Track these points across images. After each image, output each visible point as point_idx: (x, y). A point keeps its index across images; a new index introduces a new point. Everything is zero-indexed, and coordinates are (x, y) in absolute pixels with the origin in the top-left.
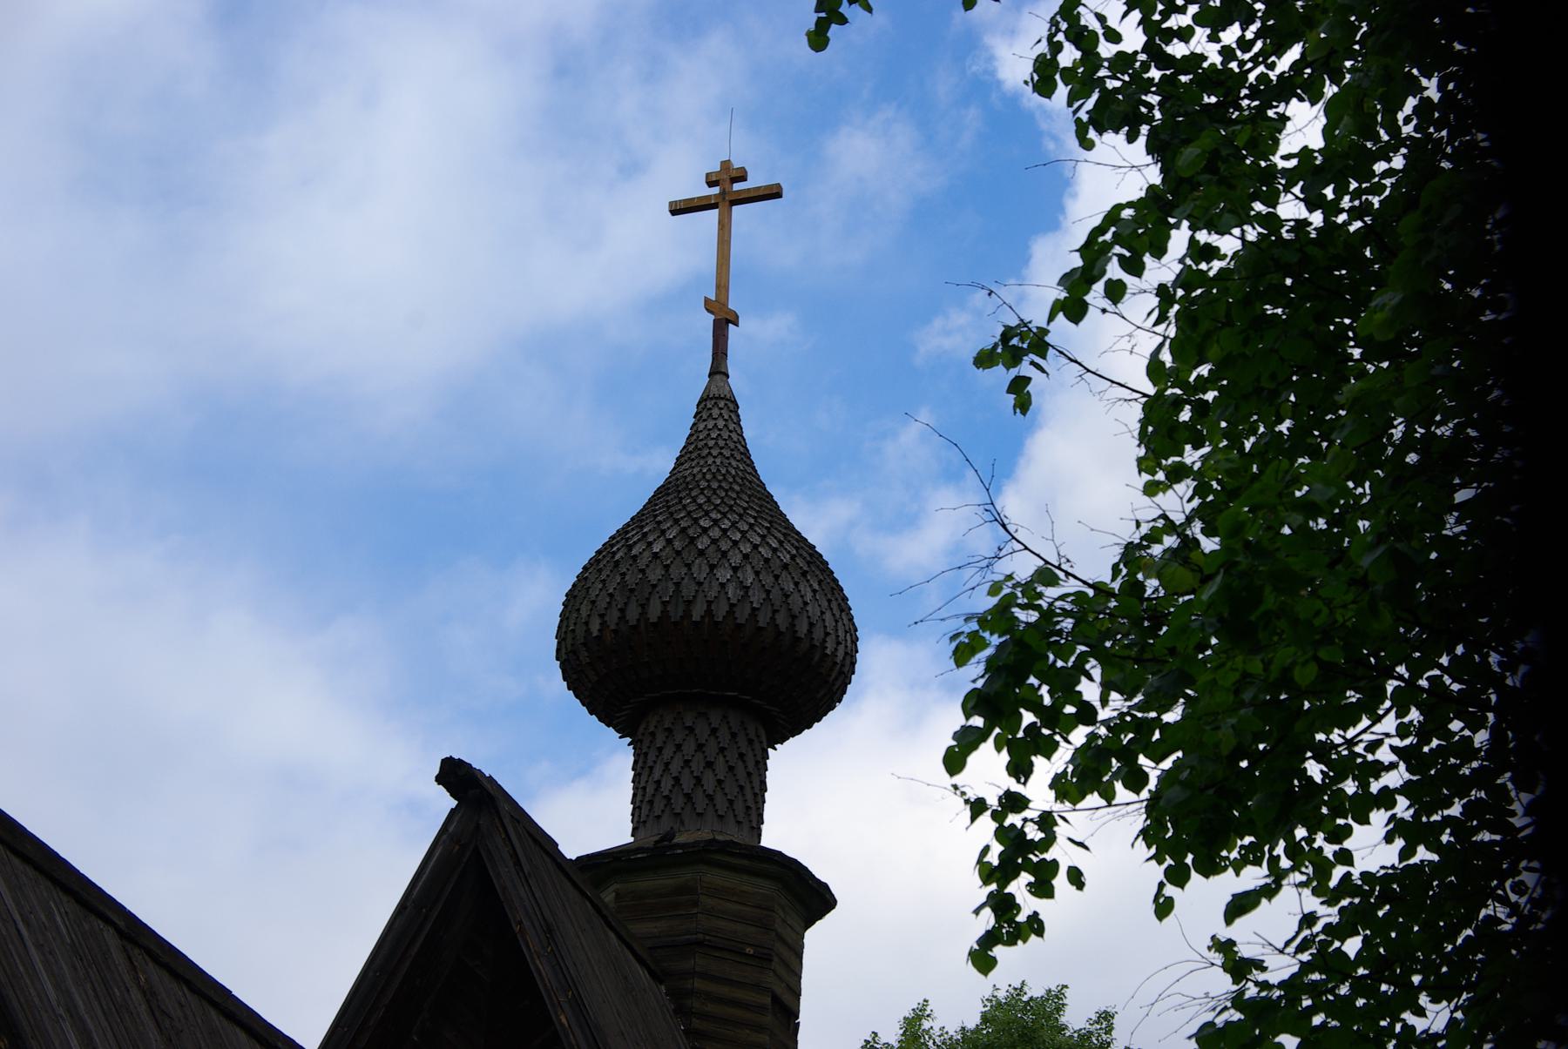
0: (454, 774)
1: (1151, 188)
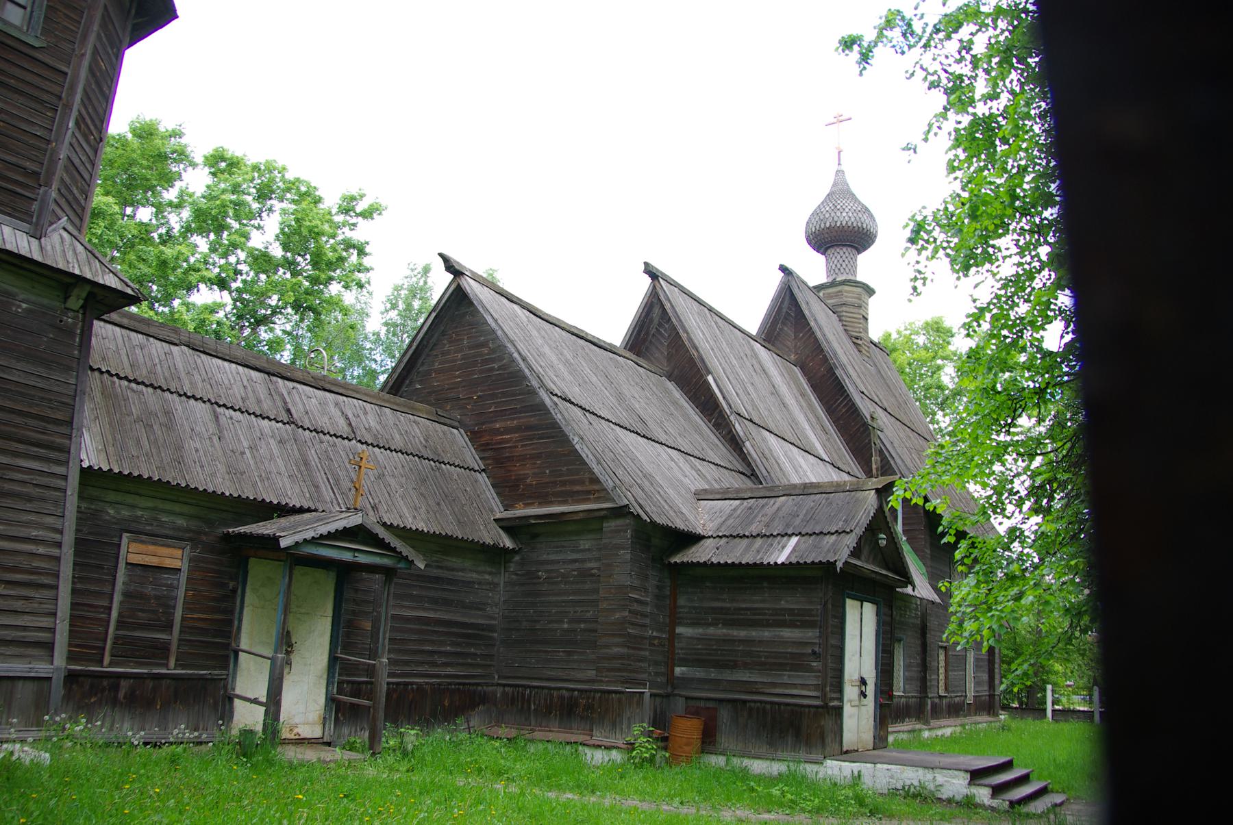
0: (783, 269)
1: (832, 565)
